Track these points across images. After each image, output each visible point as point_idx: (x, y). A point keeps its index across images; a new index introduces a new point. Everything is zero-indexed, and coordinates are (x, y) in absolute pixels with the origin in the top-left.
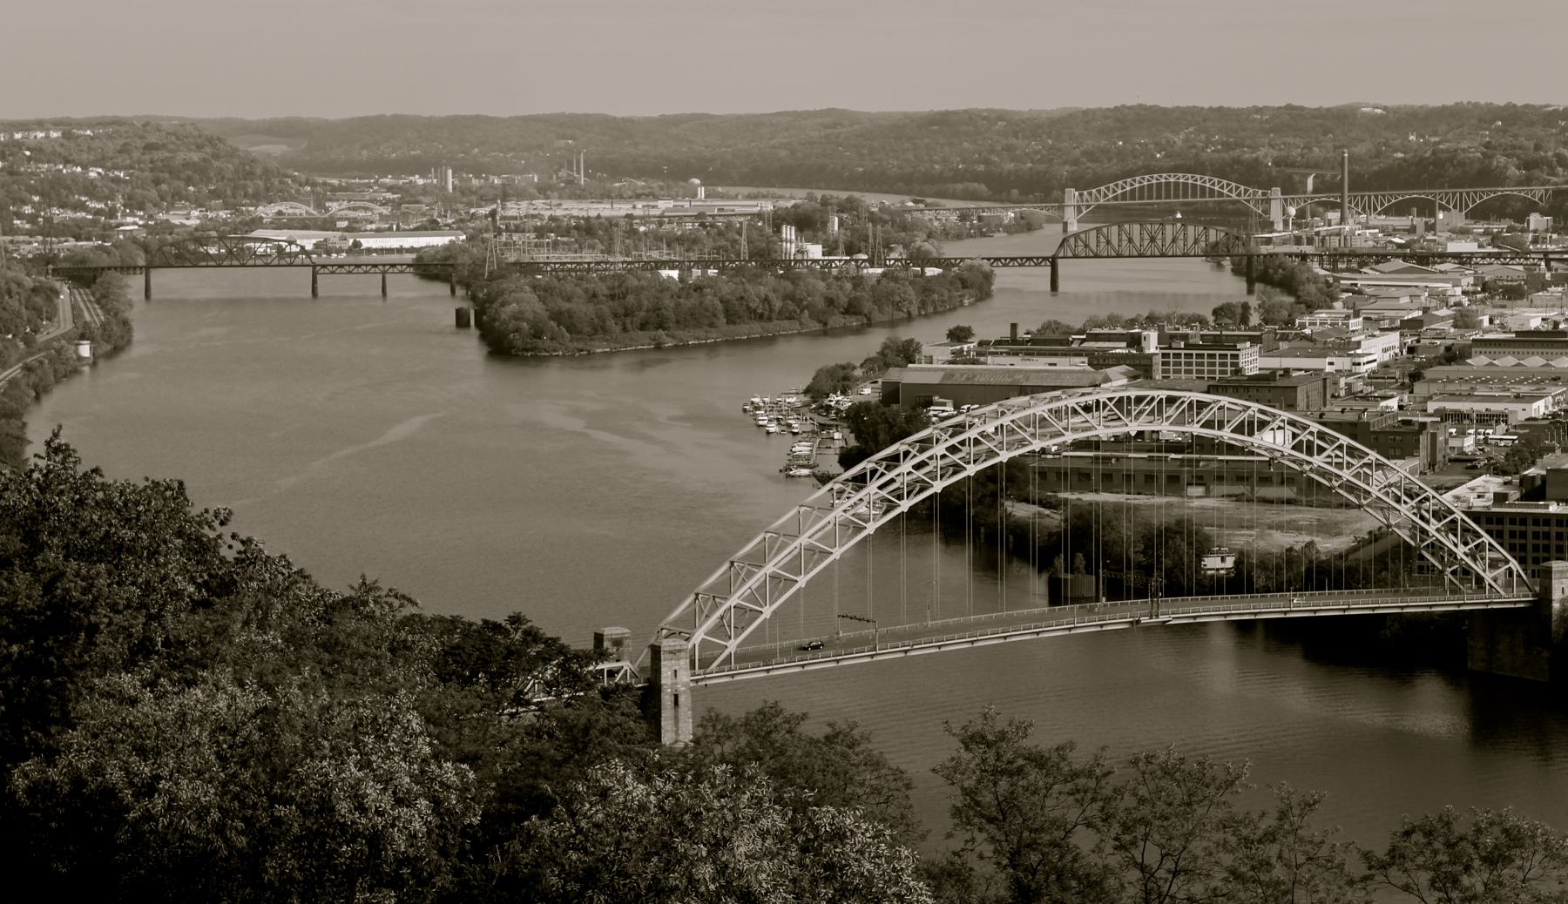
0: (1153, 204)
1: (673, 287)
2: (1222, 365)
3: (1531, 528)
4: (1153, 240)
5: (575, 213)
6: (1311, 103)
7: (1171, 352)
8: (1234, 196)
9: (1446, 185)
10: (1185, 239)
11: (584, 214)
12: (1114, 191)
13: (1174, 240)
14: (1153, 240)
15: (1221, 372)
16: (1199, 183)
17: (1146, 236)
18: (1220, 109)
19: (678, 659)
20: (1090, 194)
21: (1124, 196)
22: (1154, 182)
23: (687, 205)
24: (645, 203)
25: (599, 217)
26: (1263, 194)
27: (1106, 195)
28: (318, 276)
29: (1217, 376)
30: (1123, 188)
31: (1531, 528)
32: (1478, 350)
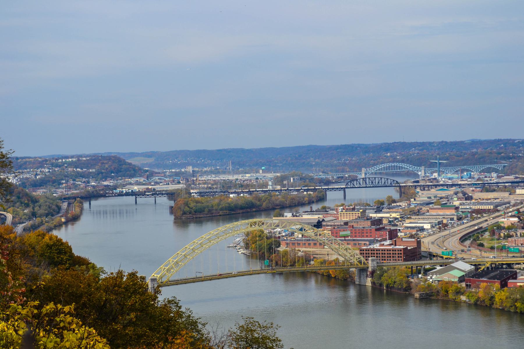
0: (403, 171)
1: (306, 196)
2: (343, 216)
3: (397, 252)
4: (372, 182)
5: (222, 178)
6: (448, 140)
7: (342, 213)
8: (411, 169)
9: (273, 172)
10: (381, 182)
11: (224, 179)
12: (376, 169)
13: (378, 182)
14: (372, 182)
15: (349, 218)
16: (401, 165)
17: (370, 182)
18: (198, 150)
19: (154, 281)
20: (369, 169)
21: (379, 170)
22: (388, 165)
23: (255, 175)
24: (242, 175)
25: (228, 179)
26: (419, 168)
27: (374, 170)
28: (137, 199)
29: (351, 219)
30: (379, 167)
31: (370, 252)
32: (431, 211)
